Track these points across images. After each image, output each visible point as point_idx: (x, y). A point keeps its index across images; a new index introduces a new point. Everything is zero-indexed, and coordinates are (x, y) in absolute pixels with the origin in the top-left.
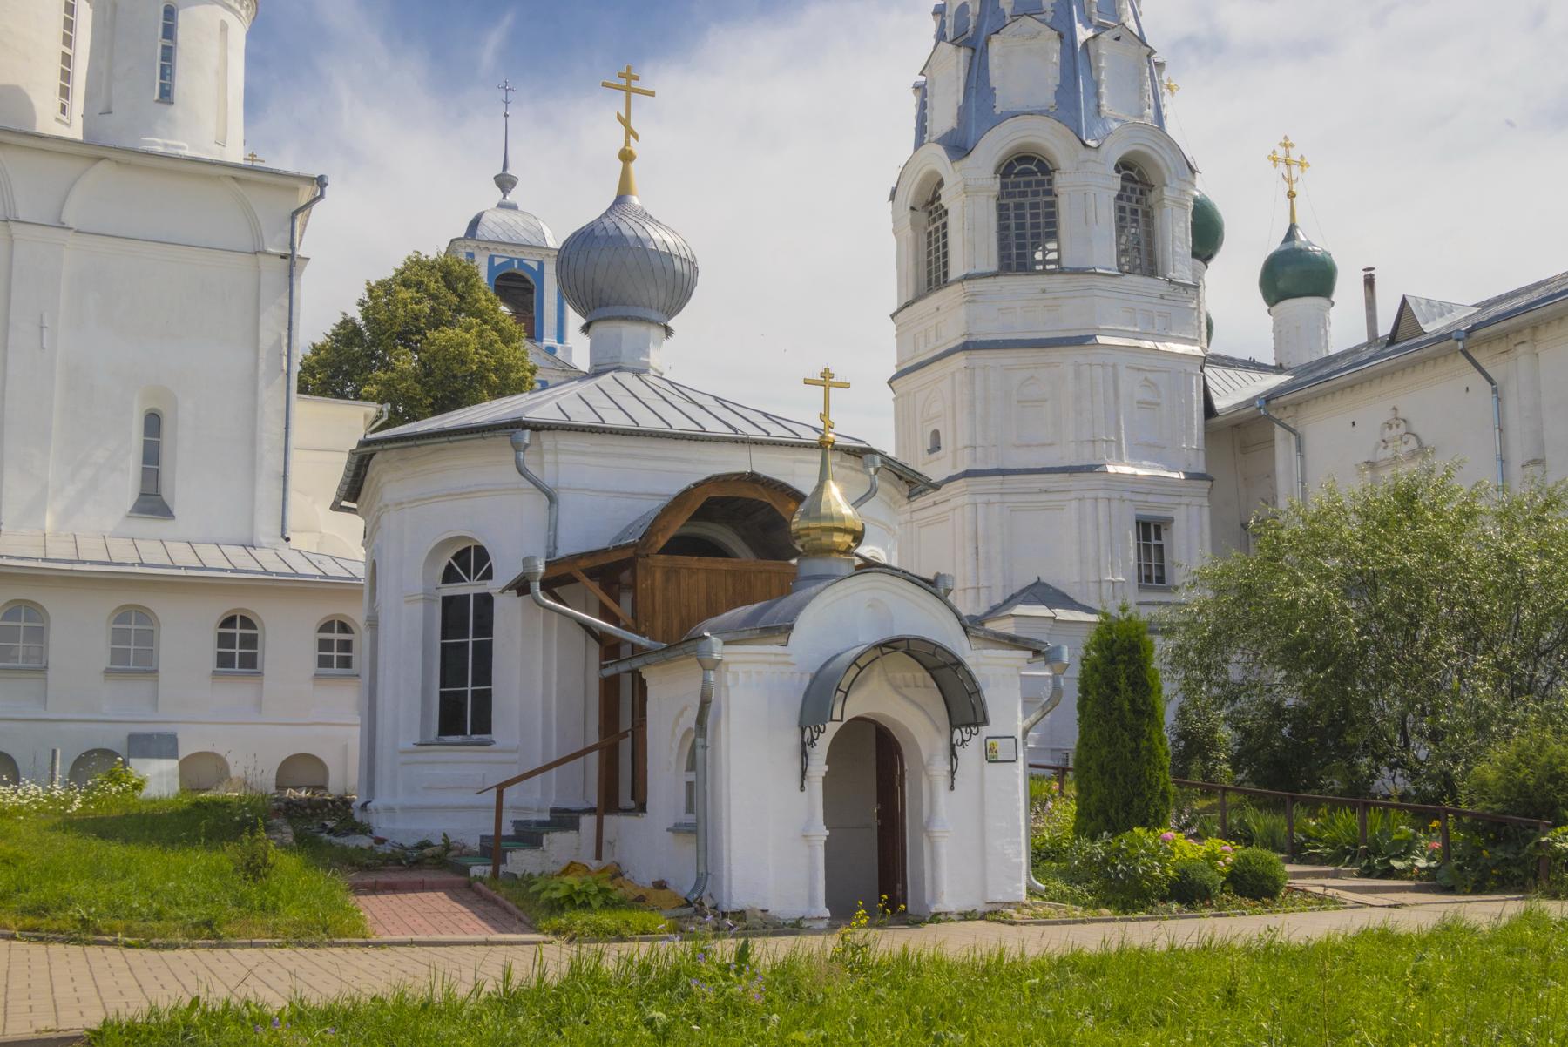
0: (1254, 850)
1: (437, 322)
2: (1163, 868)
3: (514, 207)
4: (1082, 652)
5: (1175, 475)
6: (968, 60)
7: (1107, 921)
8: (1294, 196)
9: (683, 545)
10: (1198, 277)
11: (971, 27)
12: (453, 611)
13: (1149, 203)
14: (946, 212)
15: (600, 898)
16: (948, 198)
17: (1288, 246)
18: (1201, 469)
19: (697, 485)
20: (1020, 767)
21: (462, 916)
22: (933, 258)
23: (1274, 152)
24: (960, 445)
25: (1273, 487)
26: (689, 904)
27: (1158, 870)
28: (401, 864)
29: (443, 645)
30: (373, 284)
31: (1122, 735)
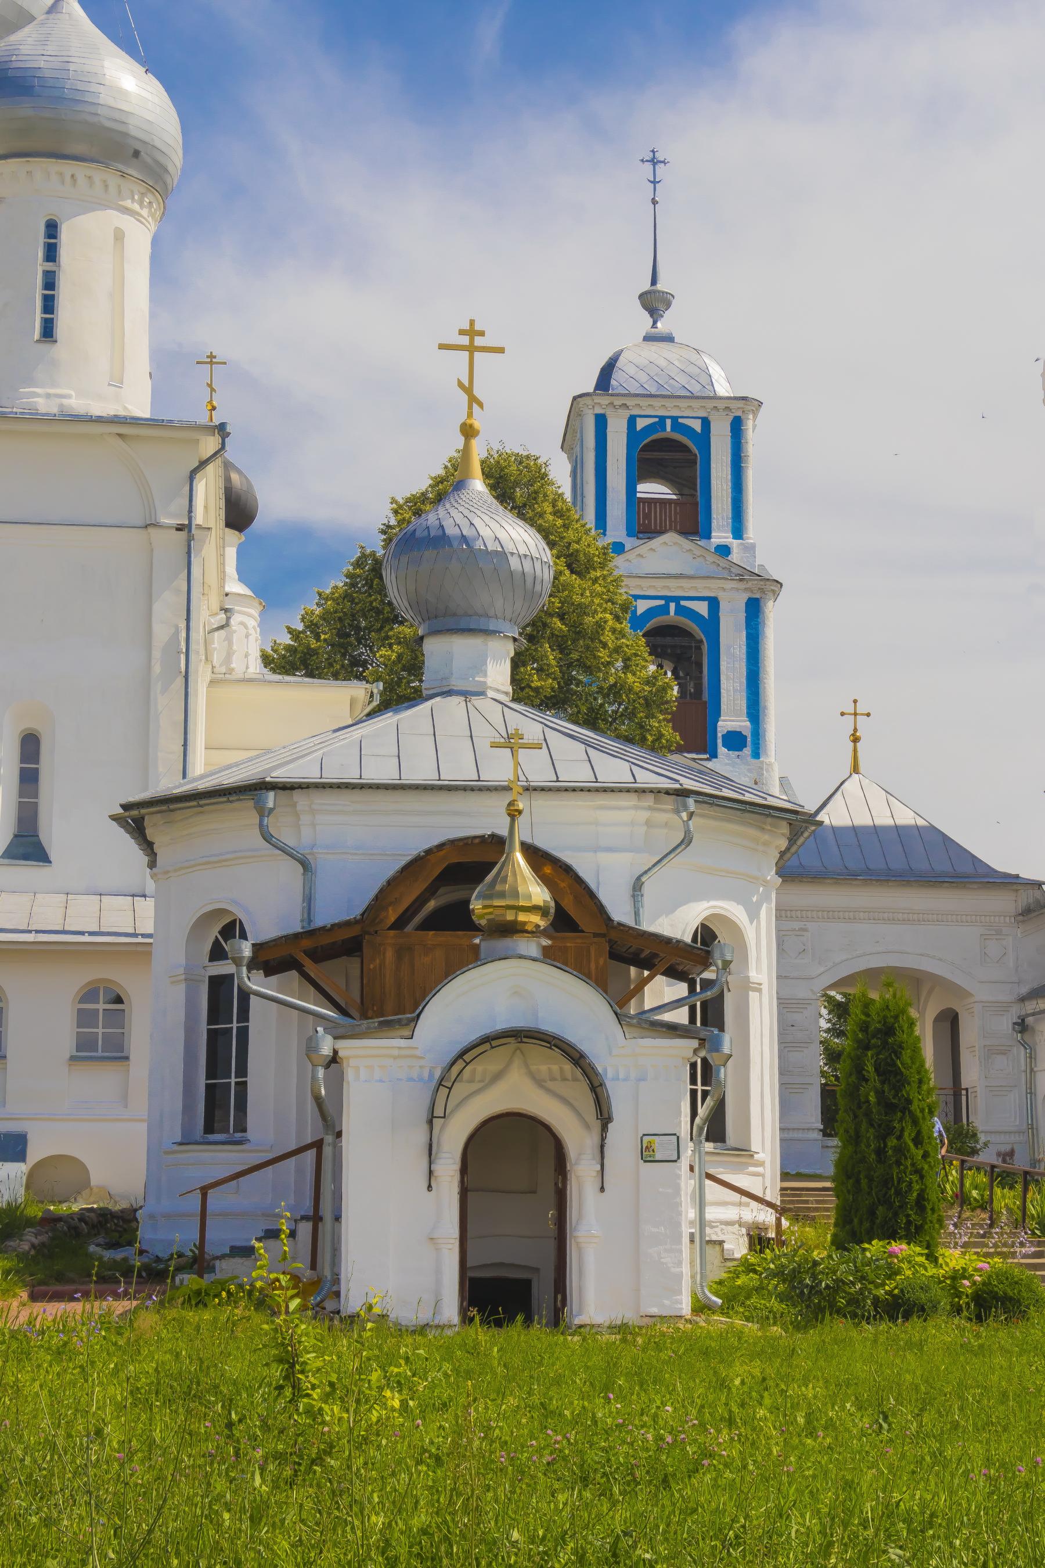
3: (669, 339)
30: (401, 502)
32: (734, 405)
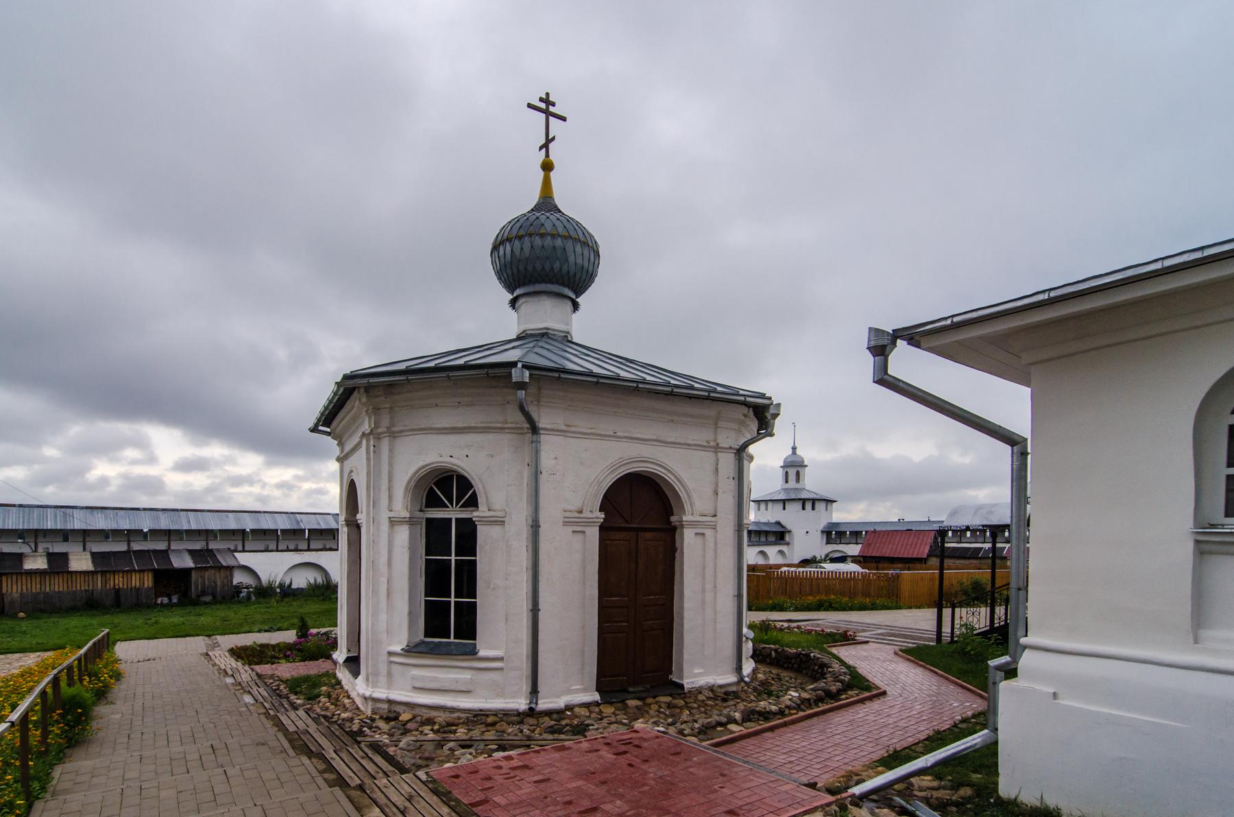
12: (435, 534)
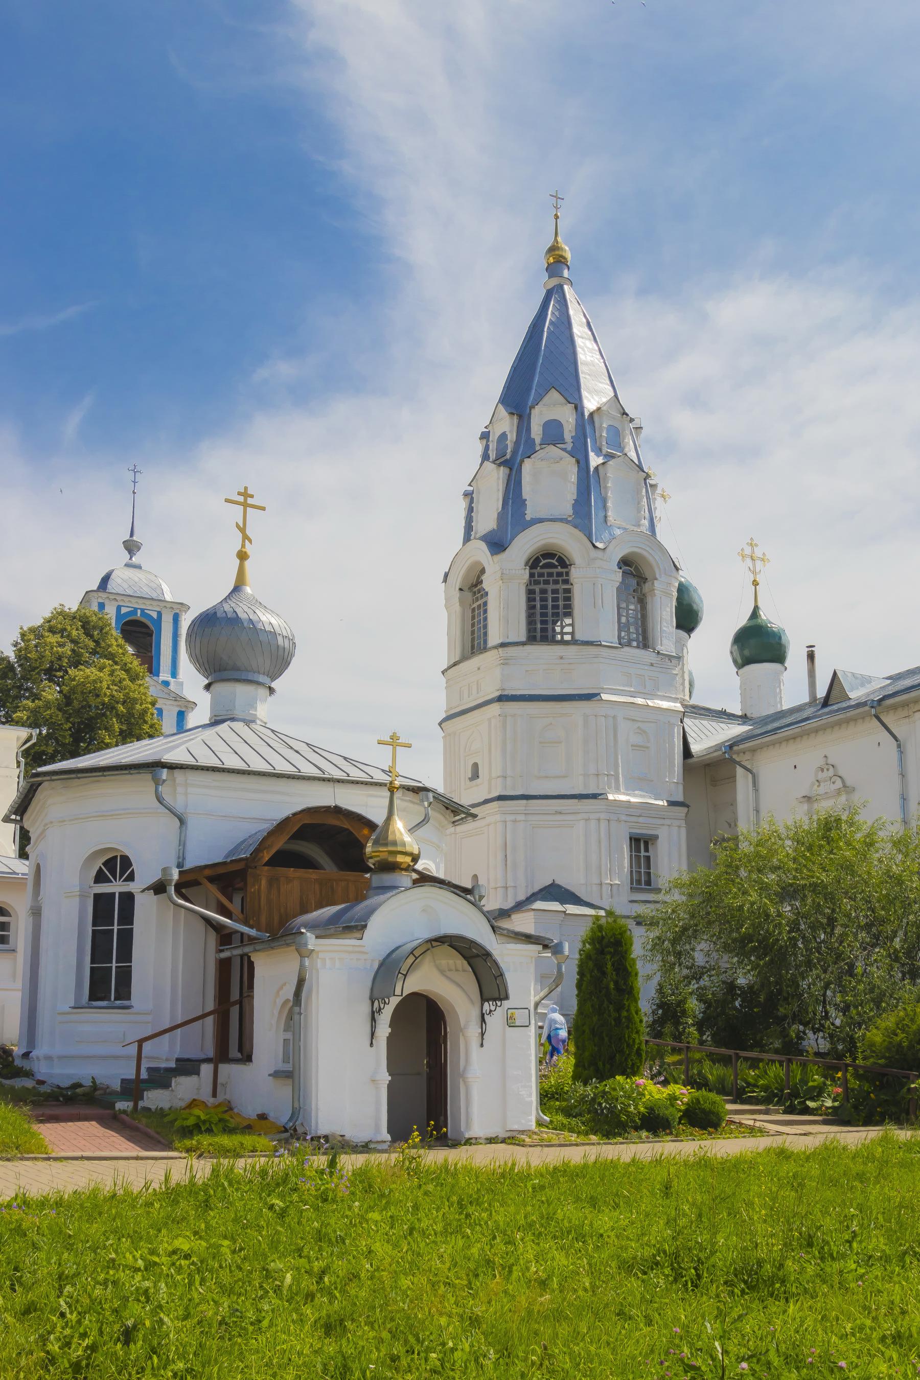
0: (704, 1092)
1: (76, 662)
2: (636, 1108)
3: (138, 567)
4: (580, 945)
5: (660, 803)
6: (506, 477)
7: (593, 1144)
8: (758, 584)
9: (283, 859)
10: (681, 645)
11: (509, 451)
12: (102, 904)
13: (644, 591)
14: (487, 594)
15: (221, 1125)
16: (489, 583)
17: (753, 623)
18: (680, 798)
19: (294, 815)
20: (532, 1031)
21: (112, 1139)
22: (476, 628)
23: (742, 550)
24: (494, 775)
25: (735, 813)
26: (286, 1131)
27: (632, 1107)
28: (58, 1100)
29: (93, 931)
31: (608, 1007)
32: (175, 606)
